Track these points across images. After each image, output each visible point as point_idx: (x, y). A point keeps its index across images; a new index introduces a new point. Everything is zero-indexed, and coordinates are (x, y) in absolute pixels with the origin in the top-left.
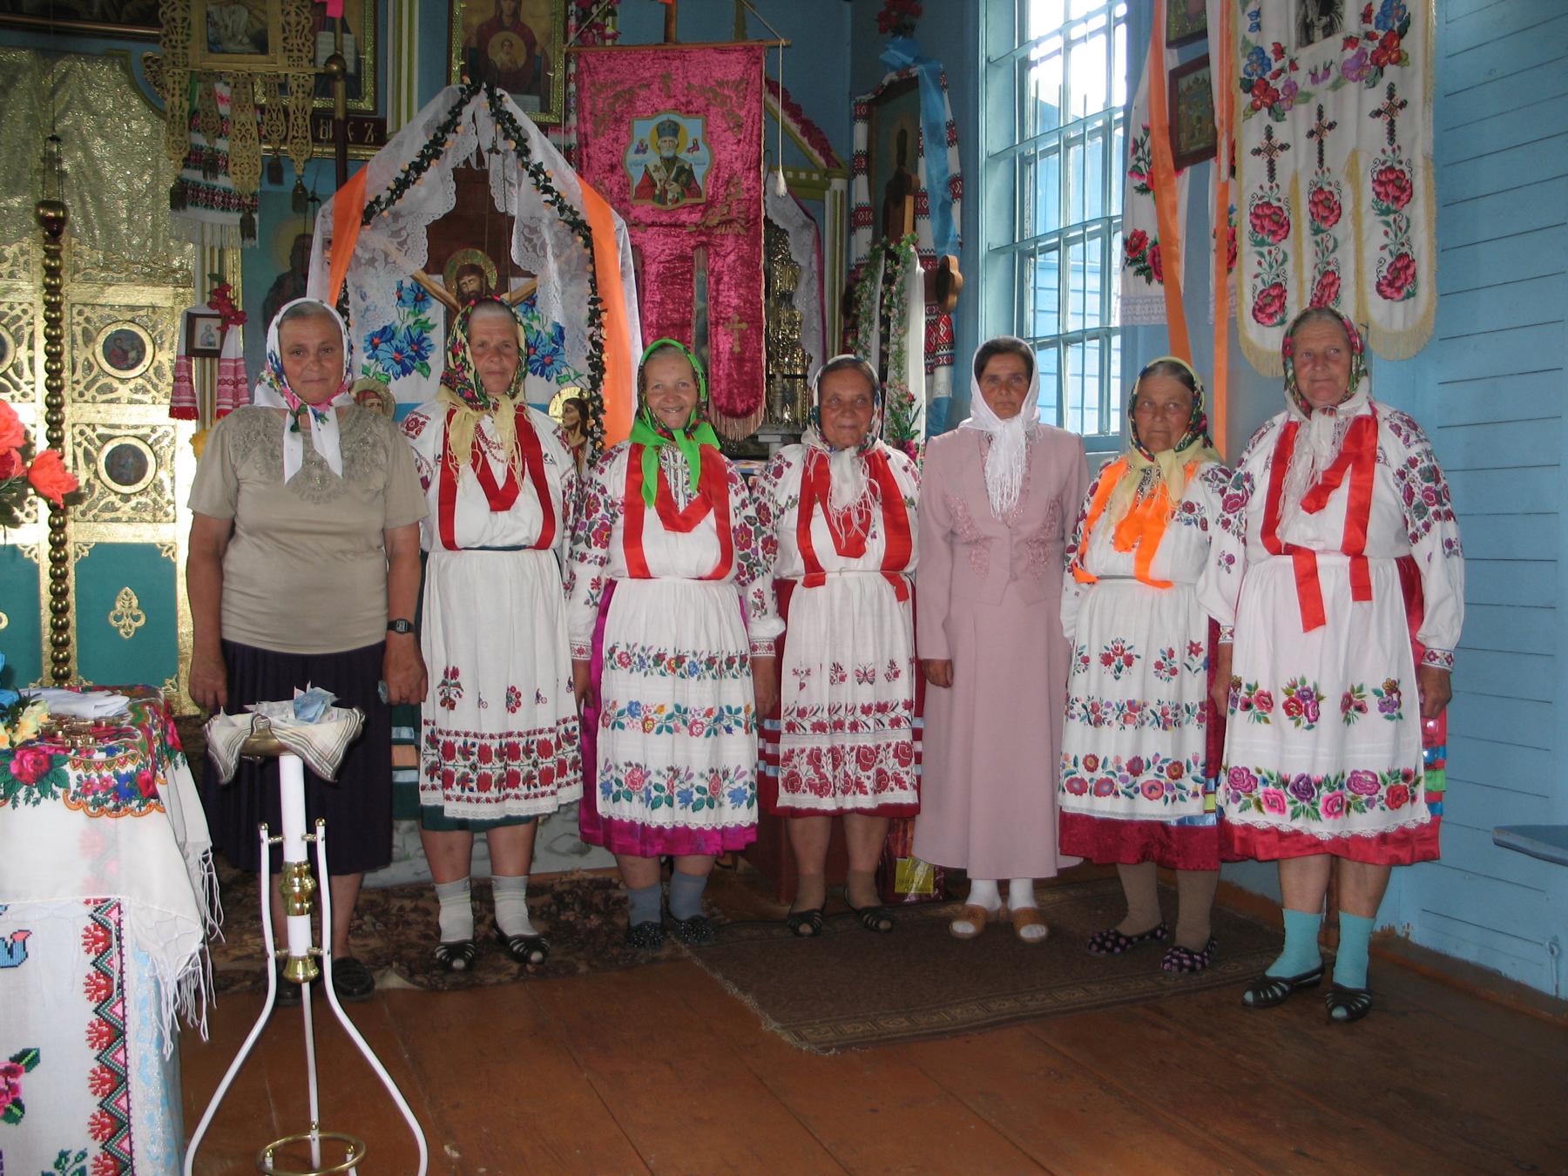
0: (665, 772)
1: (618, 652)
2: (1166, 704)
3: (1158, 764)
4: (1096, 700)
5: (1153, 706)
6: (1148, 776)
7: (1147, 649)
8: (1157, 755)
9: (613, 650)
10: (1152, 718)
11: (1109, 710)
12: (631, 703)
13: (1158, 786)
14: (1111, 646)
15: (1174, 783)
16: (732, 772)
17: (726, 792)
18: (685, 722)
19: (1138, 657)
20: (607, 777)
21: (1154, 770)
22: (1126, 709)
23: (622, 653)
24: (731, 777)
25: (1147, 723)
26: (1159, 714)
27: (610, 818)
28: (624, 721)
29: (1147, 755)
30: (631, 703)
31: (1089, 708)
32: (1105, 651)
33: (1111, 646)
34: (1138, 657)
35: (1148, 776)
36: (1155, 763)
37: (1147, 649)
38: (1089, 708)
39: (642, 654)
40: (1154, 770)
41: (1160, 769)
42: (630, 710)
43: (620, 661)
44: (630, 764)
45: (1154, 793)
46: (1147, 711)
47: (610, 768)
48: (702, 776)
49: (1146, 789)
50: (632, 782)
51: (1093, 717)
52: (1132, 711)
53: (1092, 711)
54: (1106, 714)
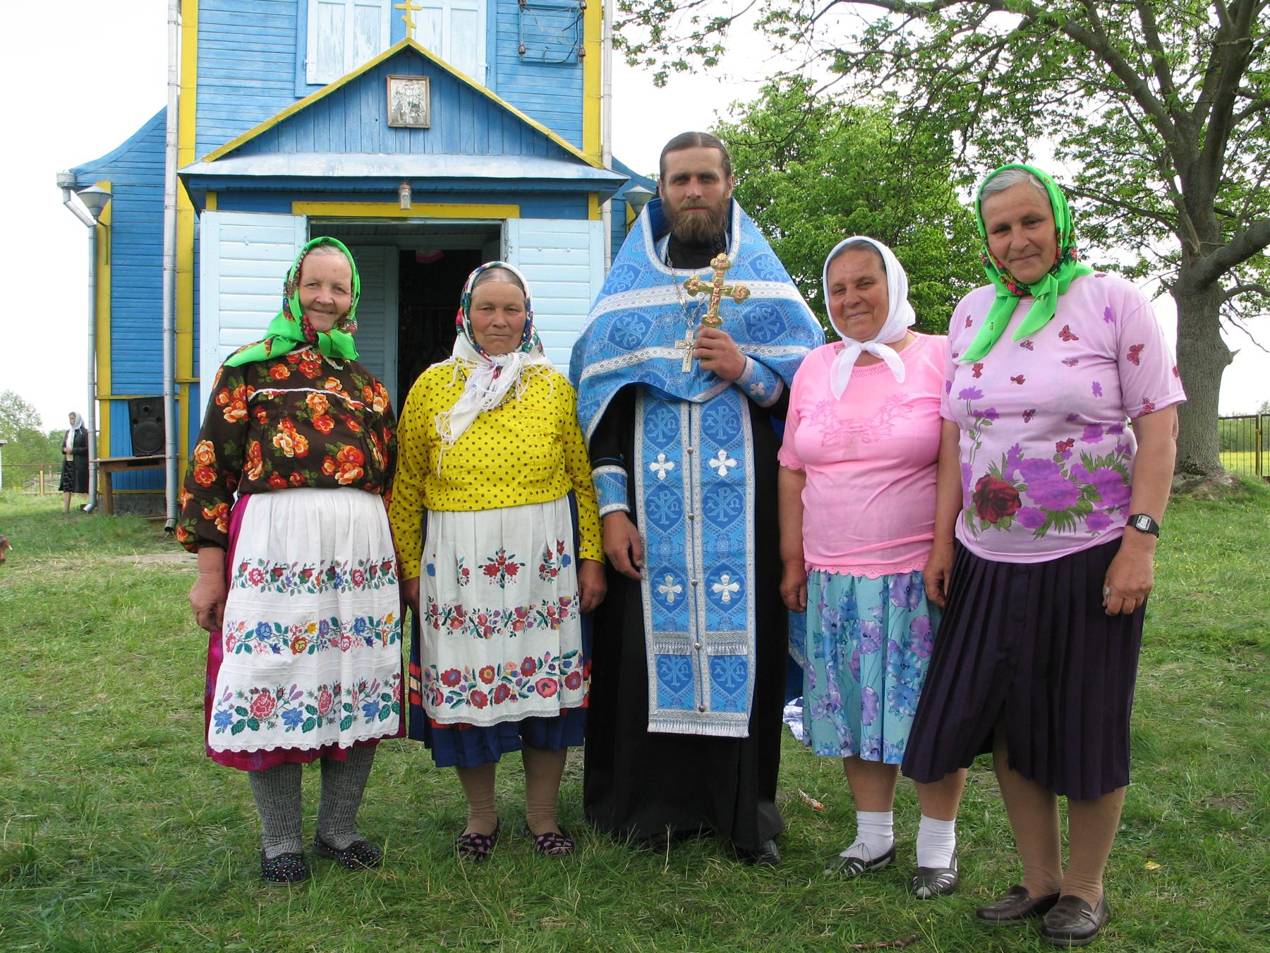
0: (248, 695)
1: (250, 568)
2: (551, 604)
3: (550, 662)
4: (483, 612)
5: (539, 607)
6: (541, 675)
7: (525, 553)
8: (548, 653)
9: (244, 566)
10: (539, 618)
11: (498, 619)
12: (260, 625)
13: (550, 683)
14: (495, 557)
15: (457, 689)
16: (287, 691)
17: (280, 712)
18: (285, 642)
19: (523, 565)
20: (225, 706)
21: (546, 668)
22: (515, 616)
23: (254, 570)
24: (286, 696)
25: (535, 624)
26: (545, 614)
27: (323, 746)
28: (253, 643)
29: (536, 655)
30: (260, 625)
31: (476, 621)
32: (489, 563)
33: (495, 557)
34: (523, 565)
35: (541, 675)
36: (546, 662)
37: (525, 553)
38: (476, 621)
39: (261, 568)
40: (546, 668)
41: (552, 667)
42: (258, 631)
43: (252, 579)
44: (256, 691)
45: (547, 691)
46: (533, 613)
47: (230, 695)
48: (311, 694)
49: (539, 686)
50: (258, 709)
51: (482, 630)
52: (520, 618)
53: (481, 623)
54: (495, 622)
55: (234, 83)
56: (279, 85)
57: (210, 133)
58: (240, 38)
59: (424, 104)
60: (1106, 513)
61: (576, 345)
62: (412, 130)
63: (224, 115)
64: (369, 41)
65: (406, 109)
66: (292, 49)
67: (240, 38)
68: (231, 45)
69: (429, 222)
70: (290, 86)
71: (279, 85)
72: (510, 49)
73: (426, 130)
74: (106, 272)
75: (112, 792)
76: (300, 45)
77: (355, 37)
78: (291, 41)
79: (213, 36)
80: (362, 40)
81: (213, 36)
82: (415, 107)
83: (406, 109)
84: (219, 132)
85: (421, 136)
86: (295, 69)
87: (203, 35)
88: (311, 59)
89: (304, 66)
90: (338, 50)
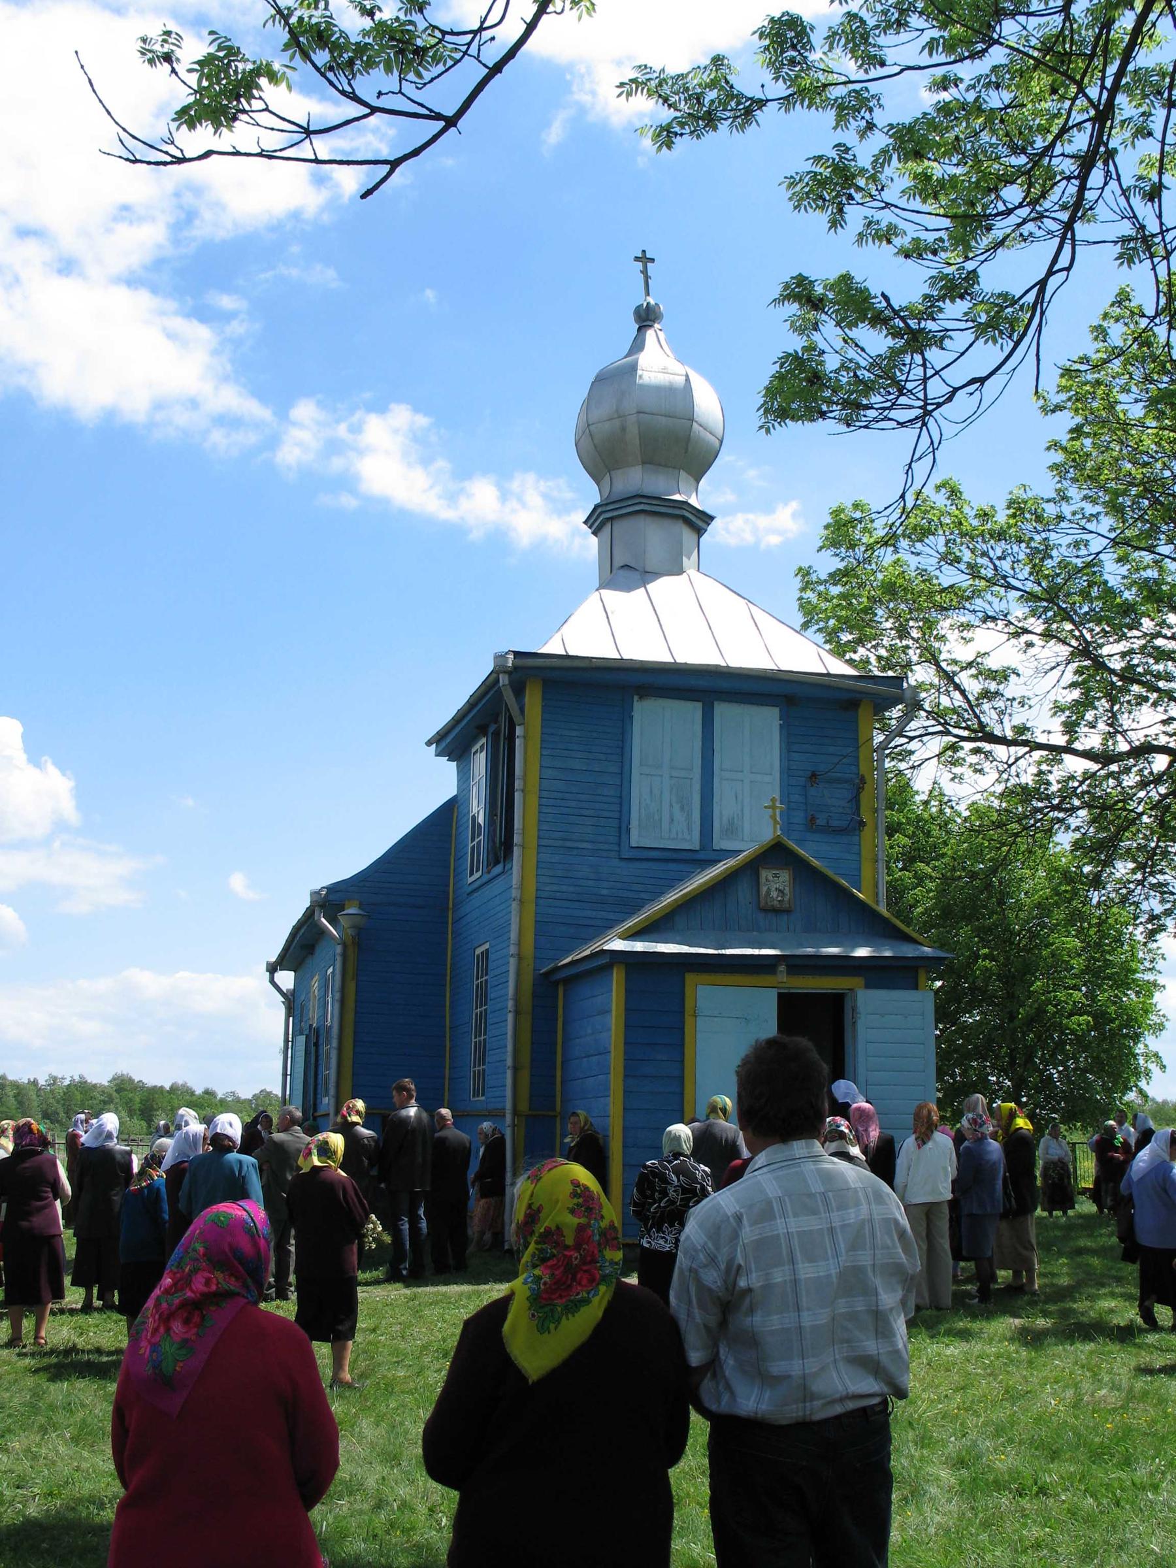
55: (568, 844)
56: (606, 847)
57: (547, 889)
58: (573, 804)
59: (787, 891)
60: (1121, 1151)
61: (333, 889)
62: (776, 911)
63: (559, 873)
64: (682, 808)
65: (774, 894)
66: (616, 815)
67: (573, 804)
68: (566, 811)
69: (792, 991)
70: (616, 848)
71: (606, 847)
72: (799, 817)
73: (788, 911)
74: (352, 987)
75: (1123, 1554)
76: (625, 808)
77: (671, 805)
78: (616, 807)
79: (551, 802)
80: (676, 807)
81: (551, 802)
82: (781, 891)
83: (774, 894)
84: (555, 888)
85: (785, 917)
86: (620, 832)
87: (544, 801)
88: (634, 823)
89: (628, 831)
90: (656, 817)
